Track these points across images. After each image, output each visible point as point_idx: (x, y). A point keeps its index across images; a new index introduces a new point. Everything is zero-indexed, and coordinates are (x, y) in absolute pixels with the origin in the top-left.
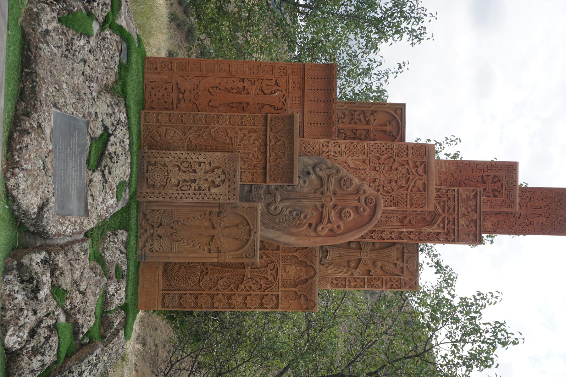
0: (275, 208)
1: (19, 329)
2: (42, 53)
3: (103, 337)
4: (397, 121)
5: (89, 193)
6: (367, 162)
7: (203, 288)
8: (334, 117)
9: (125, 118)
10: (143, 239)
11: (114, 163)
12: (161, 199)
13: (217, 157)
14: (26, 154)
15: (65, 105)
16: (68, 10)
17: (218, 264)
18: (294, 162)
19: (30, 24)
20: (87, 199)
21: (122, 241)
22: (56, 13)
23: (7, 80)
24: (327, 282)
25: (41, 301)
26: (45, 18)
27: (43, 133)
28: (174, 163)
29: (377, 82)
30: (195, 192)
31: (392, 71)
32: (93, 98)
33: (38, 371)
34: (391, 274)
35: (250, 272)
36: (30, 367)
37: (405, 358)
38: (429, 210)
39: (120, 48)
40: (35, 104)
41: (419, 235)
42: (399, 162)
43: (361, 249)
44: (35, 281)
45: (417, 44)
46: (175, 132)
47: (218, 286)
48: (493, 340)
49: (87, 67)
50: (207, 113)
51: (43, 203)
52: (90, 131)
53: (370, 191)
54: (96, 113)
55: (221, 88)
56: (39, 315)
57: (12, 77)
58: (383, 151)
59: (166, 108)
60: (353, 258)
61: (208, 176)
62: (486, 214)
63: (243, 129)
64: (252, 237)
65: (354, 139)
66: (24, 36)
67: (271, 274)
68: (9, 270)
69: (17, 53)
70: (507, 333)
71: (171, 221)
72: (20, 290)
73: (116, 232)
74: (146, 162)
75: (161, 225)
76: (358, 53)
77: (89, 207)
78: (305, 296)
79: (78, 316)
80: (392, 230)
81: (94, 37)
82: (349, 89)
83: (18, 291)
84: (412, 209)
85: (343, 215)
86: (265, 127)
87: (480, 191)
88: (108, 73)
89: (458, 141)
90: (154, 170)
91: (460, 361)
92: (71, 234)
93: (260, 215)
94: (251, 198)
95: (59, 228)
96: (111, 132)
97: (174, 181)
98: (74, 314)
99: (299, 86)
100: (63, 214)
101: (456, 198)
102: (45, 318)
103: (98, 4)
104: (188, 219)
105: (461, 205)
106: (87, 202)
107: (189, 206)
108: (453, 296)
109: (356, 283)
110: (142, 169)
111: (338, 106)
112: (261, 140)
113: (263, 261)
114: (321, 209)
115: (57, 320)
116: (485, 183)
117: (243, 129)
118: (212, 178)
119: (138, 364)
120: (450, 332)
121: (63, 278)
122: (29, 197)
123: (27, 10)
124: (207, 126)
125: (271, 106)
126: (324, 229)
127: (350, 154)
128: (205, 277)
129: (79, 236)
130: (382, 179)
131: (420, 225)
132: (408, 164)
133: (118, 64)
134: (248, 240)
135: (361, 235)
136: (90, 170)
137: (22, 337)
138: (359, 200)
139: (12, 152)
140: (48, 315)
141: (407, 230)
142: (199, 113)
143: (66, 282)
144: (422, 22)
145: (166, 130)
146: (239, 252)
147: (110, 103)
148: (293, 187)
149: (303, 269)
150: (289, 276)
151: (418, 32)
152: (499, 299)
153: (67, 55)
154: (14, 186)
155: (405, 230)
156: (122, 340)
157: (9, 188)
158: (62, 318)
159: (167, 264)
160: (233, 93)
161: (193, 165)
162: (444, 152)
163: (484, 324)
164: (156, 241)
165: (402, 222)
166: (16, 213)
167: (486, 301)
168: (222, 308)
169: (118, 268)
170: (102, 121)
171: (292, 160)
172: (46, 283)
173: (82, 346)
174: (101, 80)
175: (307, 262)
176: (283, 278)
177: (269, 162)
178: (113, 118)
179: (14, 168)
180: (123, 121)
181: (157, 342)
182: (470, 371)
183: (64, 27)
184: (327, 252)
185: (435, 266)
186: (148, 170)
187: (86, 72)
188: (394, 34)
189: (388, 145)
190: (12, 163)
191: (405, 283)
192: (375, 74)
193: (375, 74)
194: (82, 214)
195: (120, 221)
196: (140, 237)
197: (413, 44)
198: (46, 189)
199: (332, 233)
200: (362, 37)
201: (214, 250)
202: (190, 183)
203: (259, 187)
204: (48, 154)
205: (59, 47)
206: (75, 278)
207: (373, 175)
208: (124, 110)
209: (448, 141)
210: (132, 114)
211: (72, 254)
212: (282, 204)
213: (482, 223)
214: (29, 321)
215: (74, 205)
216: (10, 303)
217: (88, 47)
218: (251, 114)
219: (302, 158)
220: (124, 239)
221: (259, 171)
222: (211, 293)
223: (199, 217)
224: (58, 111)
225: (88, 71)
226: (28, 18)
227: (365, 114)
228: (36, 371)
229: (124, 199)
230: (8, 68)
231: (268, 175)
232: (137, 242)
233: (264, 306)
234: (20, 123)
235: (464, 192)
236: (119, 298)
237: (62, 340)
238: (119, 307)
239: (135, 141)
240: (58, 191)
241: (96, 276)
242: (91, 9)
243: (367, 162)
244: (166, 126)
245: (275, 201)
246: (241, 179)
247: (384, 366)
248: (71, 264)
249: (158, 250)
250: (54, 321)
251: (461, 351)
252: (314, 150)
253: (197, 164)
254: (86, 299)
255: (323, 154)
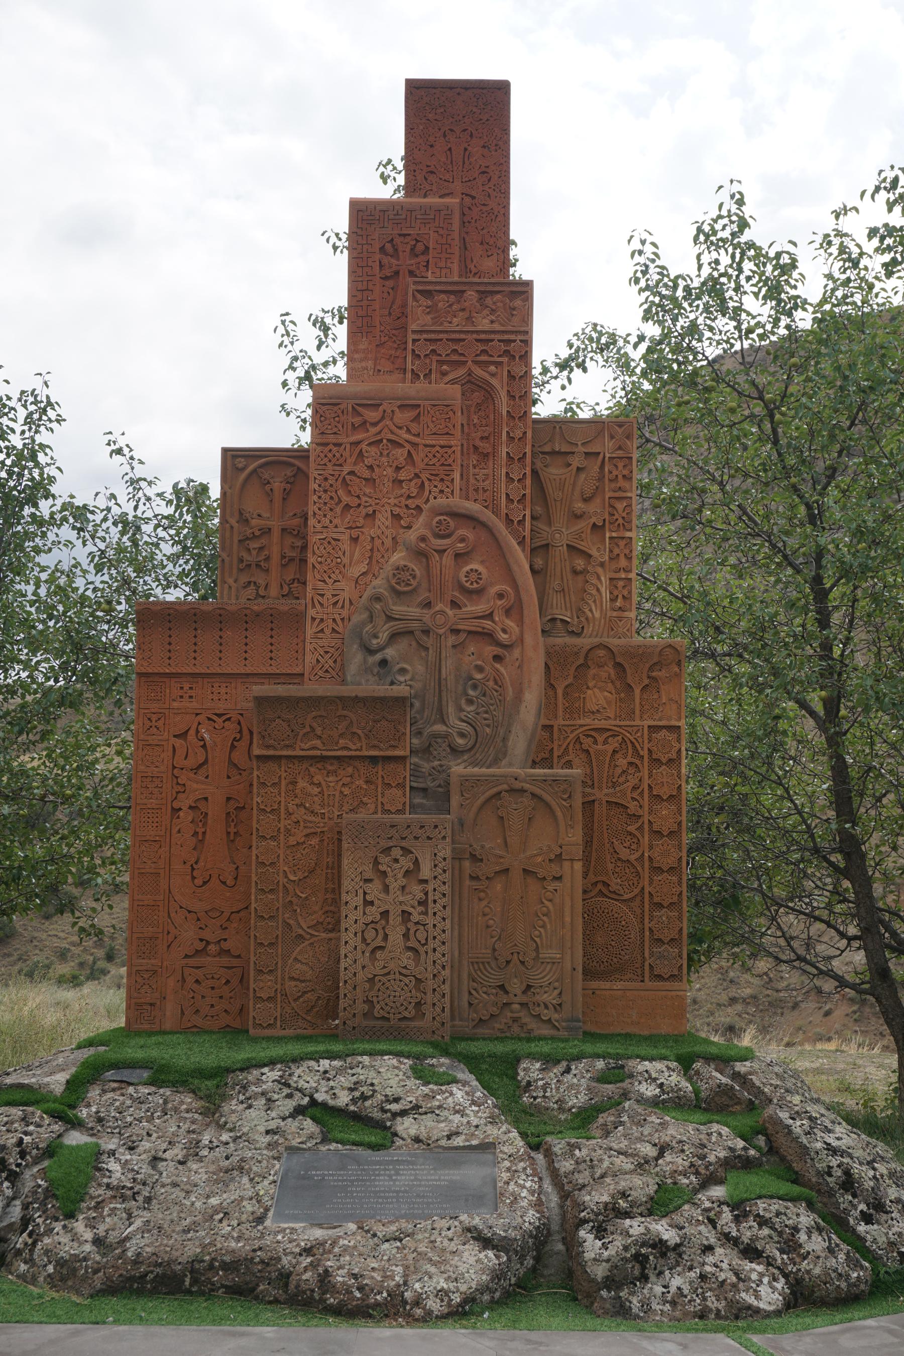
0: (462, 735)
1: (744, 1281)
2: (148, 1249)
3: (751, 1107)
4: (261, 466)
5: (443, 1142)
6: (354, 533)
7: (636, 891)
8: (256, 608)
9: (272, 1070)
10: (532, 1024)
11: (374, 1091)
12: (446, 988)
13: (353, 867)
14: (372, 1278)
15: (258, 1199)
16: (46, 1198)
17: (586, 860)
18: (360, 695)
19: (85, 1278)
20: (457, 1148)
21: (543, 1069)
22: (55, 1224)
23: (214, 1322)
24: (620, 618)
25: (684, 1237)
26: (67, 1247)
27: (322, 1244)
28: (367, 961)
29: (154, 504)
30: (430, 912)
31: (129, 471)
32: (235, 1139)
33: (830, 1239)
34: (601, 479)
35: (600, 788)
36: (823, 1255)
37: (776, 442)
38: (459, 396)
39: (115, 1085)
40: (262, 1262)
41: (513, 418)
42: (355, 464)
43: (547, 545)
44: (643, 1251)
45: (59, 411)
46: (296, 959)
47: (632, 858)
48: (735, 249)
49: (167, 1155)
50: (253, 890)
51: (473, 1238)
52: (309, 1145)
53: (420, 526)
54: (268, 1132)
55: (193, 860)
56: (713, 1241)
57: (206, 1312)
58: (331, 498)
59: (241, 981)
60: (568, 563)
61: (394, 885)
62: (465, 270)
63: (287, 809)
64: (527, 786)
65: (304, 561)
66: (111, 1290)
67: (605, 742)
68: (621, 1306)
69: (151, 1305)
70: (720, 217)
71: (493, 965)
72: (661, 1281)
73: (524, 1083)
74: (365, 1023)
75: (502, 987)
76: (95, 549)
77: (475, 1142)
78: (651, 669)
79: (712, 1158)
80: (503, 478)
81: (100, 1141)
82: (170, 566)
83: (664, 1287)
84: (458, 432)
85: (475, 585)
86: (283, 761)
87: (415, 283)
88: (176, 1110)
89: (288, 318)
90: (382, 1003)
91: (783, 324)
92: (536, 1179)
93: (476, 769)
94: (440, 789)
95: (525, 1203)
96: (307, 1099)
97: (407, 959)
98: (707, 1168)
99: (186, 686)
100: (493, 1197)
101: (433, 336)
102: (719, 1227)
103: (26, 1133)
104: (488, 927)
105: (446, 327)
106: (464, 1148)
107: (460, 926)
108: (641, 338)
109: (622, 556)
110: (382, 1029)
111: (229, 599)
112: (312, 769)
113: (576, 761)
114: (463, 636)
115: (721, 1203)
116: (397, 273)
117: (287, 809)
118: (400, 875)
119: (786, 1039)
120: (718, 343)
121: (632, 1193)
122: (462, 1268)
123: (53, 1286)
124: (281, 887)
125: (233, 747)
126: (506, 628)
127: (337, 572)
128: (614, 887)
129: (538, 1162)
130: (392, 501)
131: (492, 416)
132: (358, 443)
133: (153, 1089)
134: (533, 795)
135: (517, 547)
136: (393, 1142)
137: (761, 1275)
138: (441, 552)
139: (368, 1306)
140: (712, 1222)
141: (504, 446)
142: (253, 906)
143: (642, 1186)
144: (9, 398)
145: (292, 979)
146: (559, 814)
147: (242, 1102)
148: (415, 697)
149: (592, 672)
150: (609, 703)
151: (32, 408)
152: (645, 236)
153: (145, 1197)
154: (442, 1301)
155: (505, 450)
156: (756, 1065)
157: (446, 1311)
158: (718, 1192)
159: (589, 973)
160: (204, 833)
161: (370, 919)
162: (312, 351)
163: (700, 267)
164: (537, 997)
165: (486, 455)
166: (497, 1295)
167: (652, 266)
168: (680, 850)
169: (602, 1078)
170: (284, 1119)
171: (356, 699)
172: (646, 1228)
173: (772, 1150)
174: (193, 1123)
175: (578, 663)
176: (612, 716)
177: (361, 750)
178: (276, 1097)
179: (404, 1302)
180: (279, 1073)
181: (724, 998)
182: (805, 302)
183: (83, 1205)
184: (555, 619)
185: (570, 373)
186: (383, 1018)
187: (180, 1157)
188: (37, 464)
189: (316, 487)
190: (394, 1306)
191: (620, 448)
192: (136, 508)
193: (136, 508)
194: (490, 1157)
195: (498, 1075)
196: (529, 1032)
197: (60, 420)
198: (444, 1233)
199: (515, 610)
200: (44, 535)
201: (555, 869)
202: (410, 925)
203: (416, 772)
204: (368, 1231)
205: (130, 1216)
206: (630, 1167)
207: (383, 519)
208: (256, 1072)
209: (286, 342)
210: (262, 1054)
211: (581, 1176)
212: (453, 720)
213: (486, 280)
214: (726, 1261)
215: (472, 1174)
216: (690, 1301)
217: (123, 1154)
218: (255, 790)
219: (349, 678)
220: (538, 1065)
221: (380, 773)
222: (647, 875)
223: (484, 903)
224: (270, 1214)
225: (177, 1152)
226: (70, 1283)
227: (248, 539)
228: (830, 1243)
229: (451, 1067)
230: (188, 1322)
231: (390, 753)
232: (540, 1039)
233: (674, 756)
234: (304, 1292)
235: (419, 319)
236: (667, 1074)
237: (764, 1192)
238: (685, 1075)
239: (321, 1048)
240: (446, 1209)
241: (622, 1123)
242: (38, 1148)
243: (354, 533)
244: (283, 979)
245: (446, 736)
246: (399, 812)
247: (795, 489)
248: (603, 1176)
249: (556, 992)
250: (725, 1208)
251: (759, 319)
252: (332, 650)
253: (369, 909)
254: (674, 1144)
255: (340, 630)
